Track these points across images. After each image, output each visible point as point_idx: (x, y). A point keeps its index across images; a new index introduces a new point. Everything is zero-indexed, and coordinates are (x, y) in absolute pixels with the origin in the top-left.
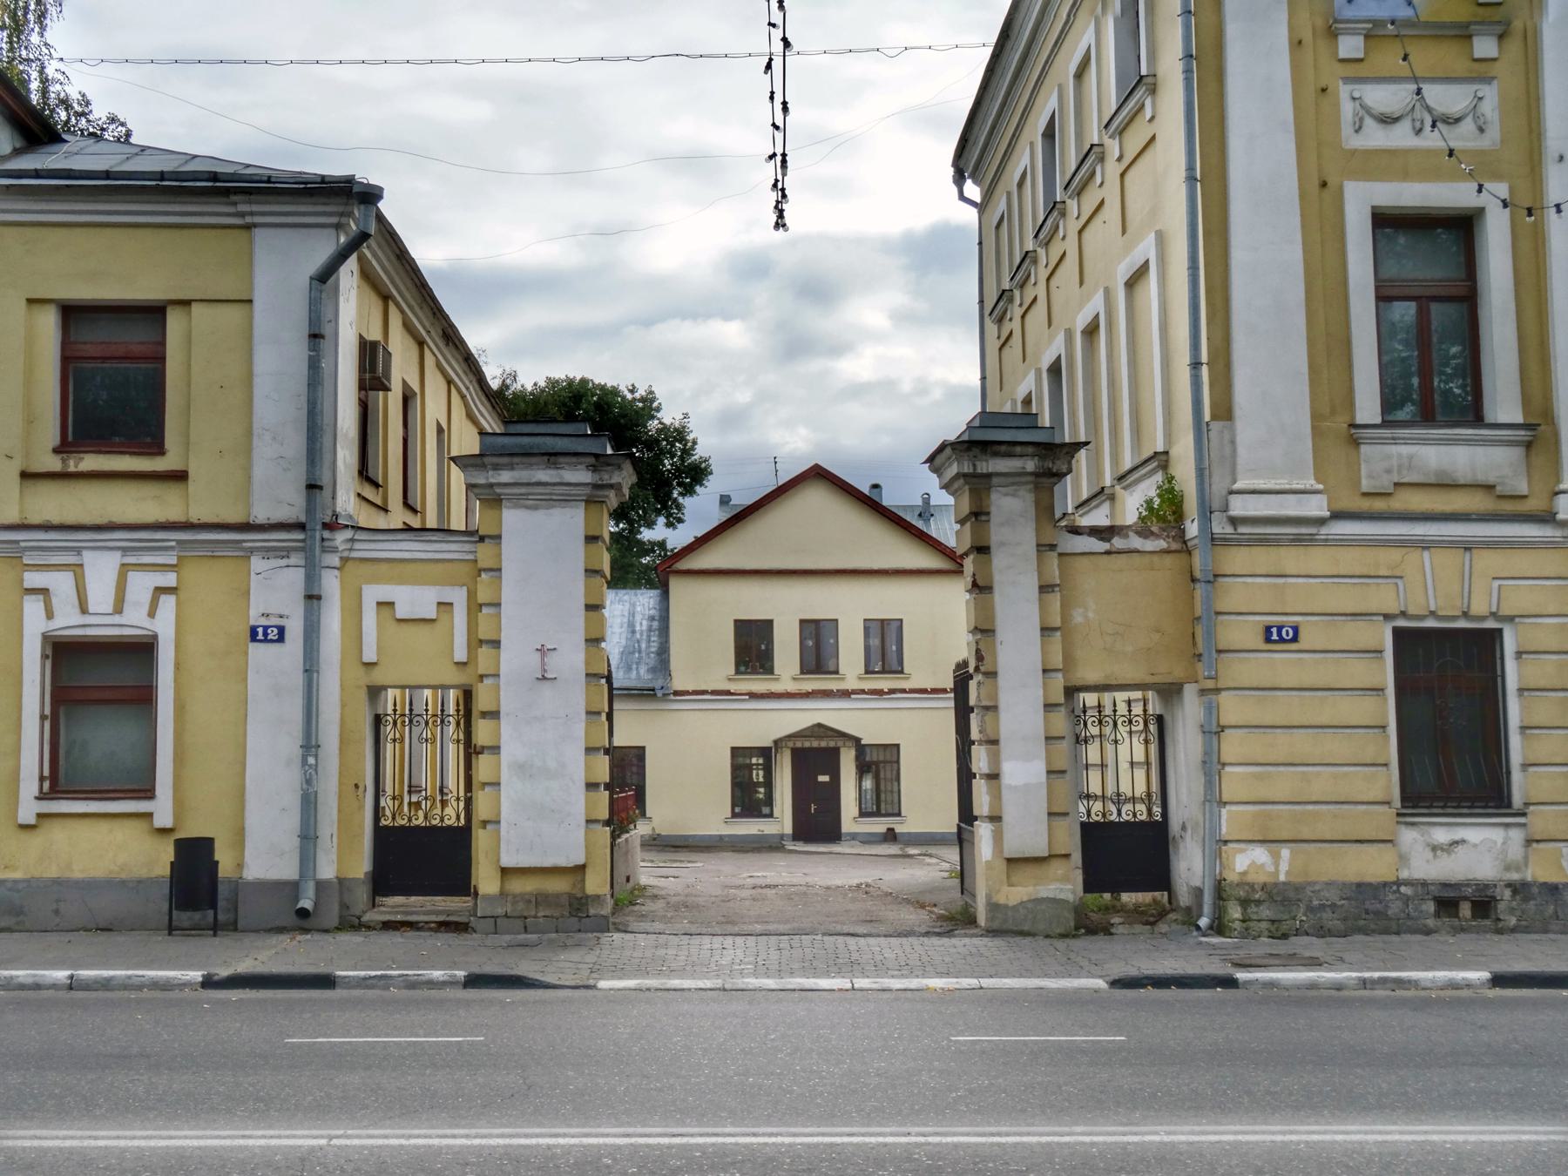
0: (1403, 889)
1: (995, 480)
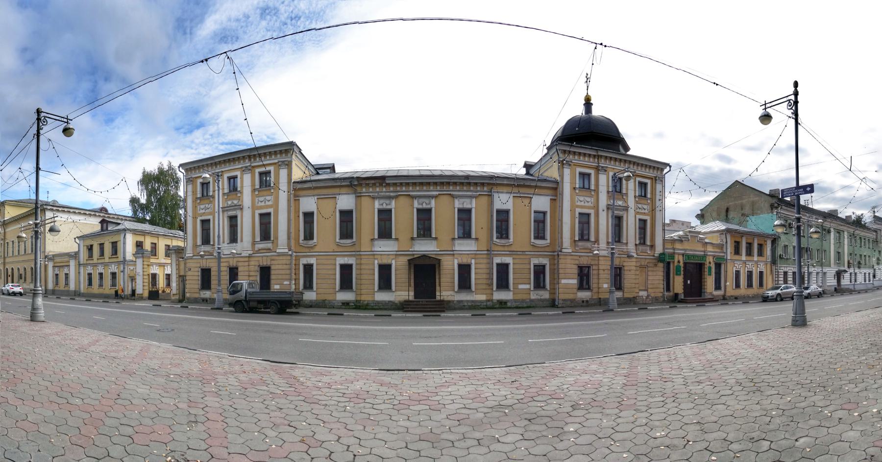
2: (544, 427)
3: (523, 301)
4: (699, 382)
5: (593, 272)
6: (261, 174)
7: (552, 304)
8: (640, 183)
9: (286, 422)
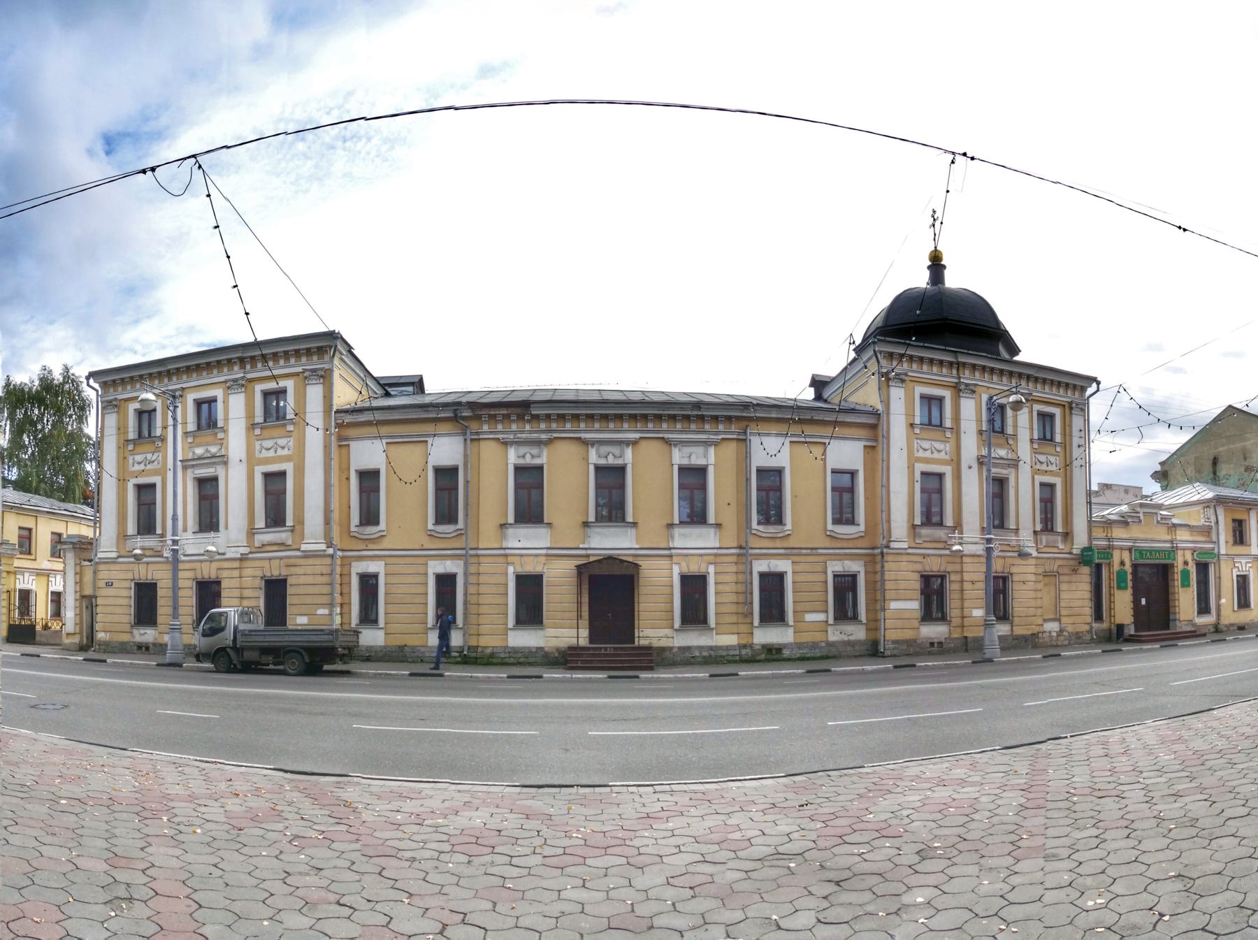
2: (868, 896)
3: (815, 645)
4: (1177, 795)
5: (952, 588)
6: (266, 394)
7: (873, 650)
8: (1042, 415)
9: (333, 898)
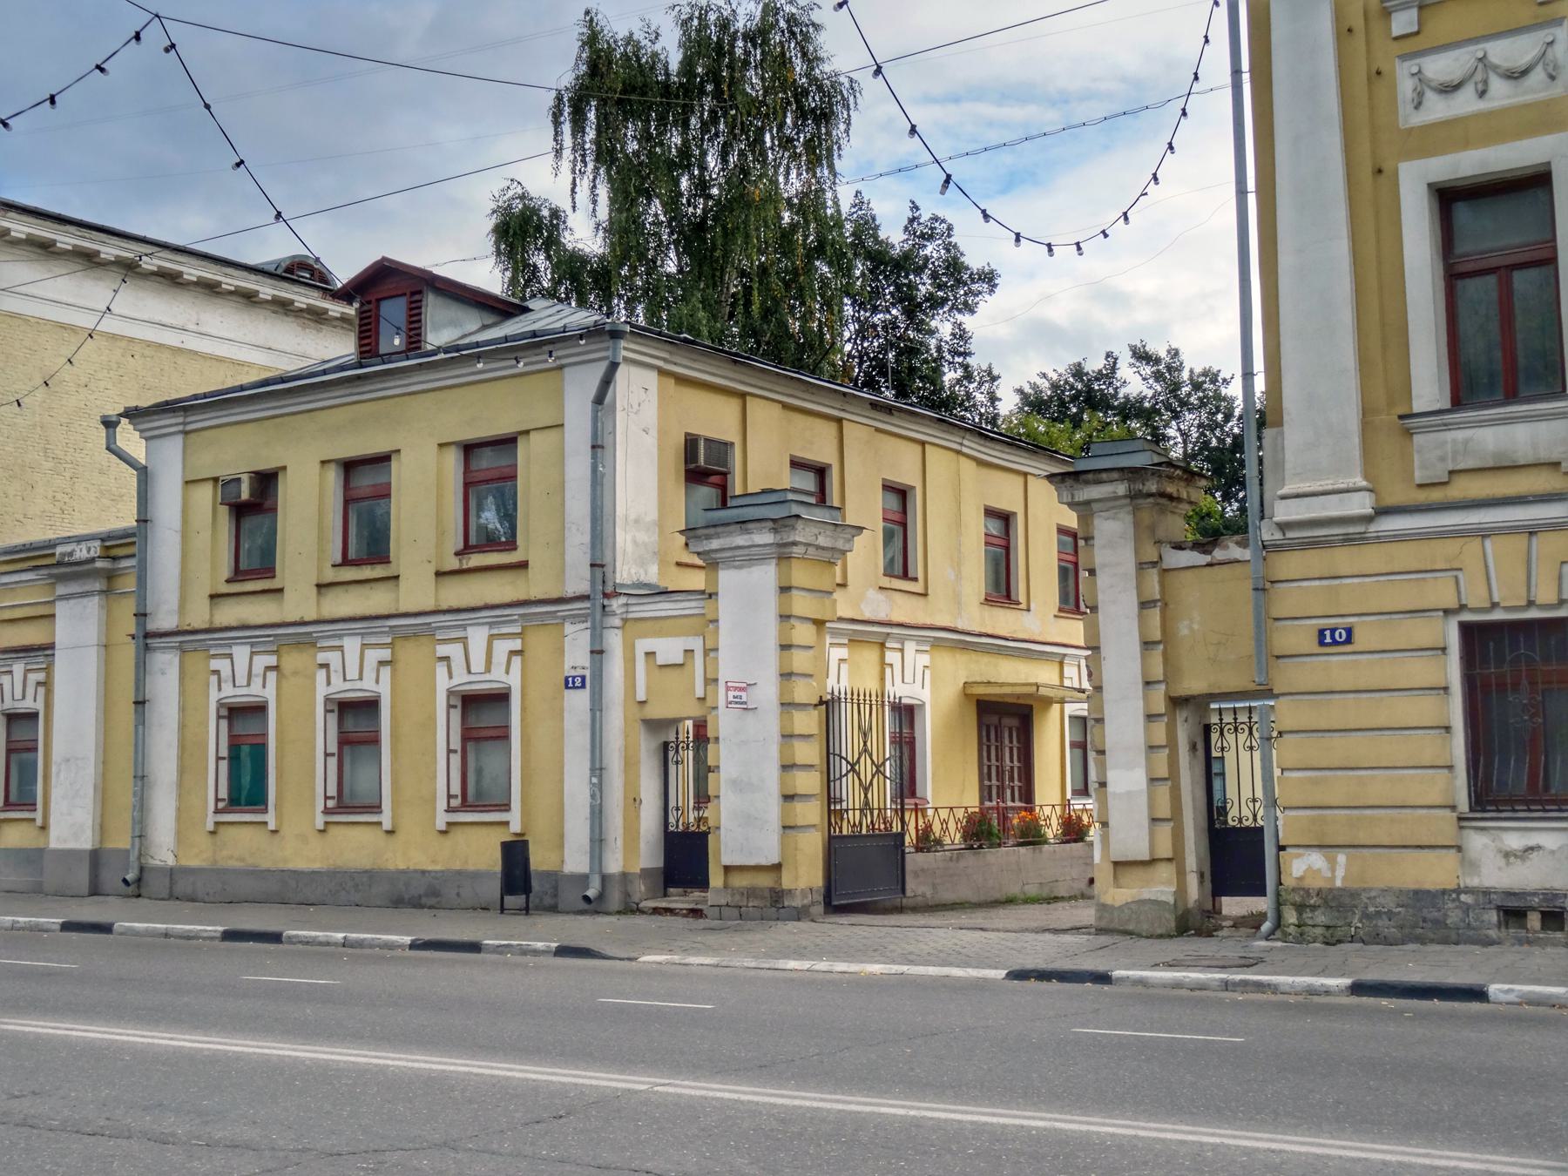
0: (1463, 897)
1: (1095, 506)
8: (905, 575)
